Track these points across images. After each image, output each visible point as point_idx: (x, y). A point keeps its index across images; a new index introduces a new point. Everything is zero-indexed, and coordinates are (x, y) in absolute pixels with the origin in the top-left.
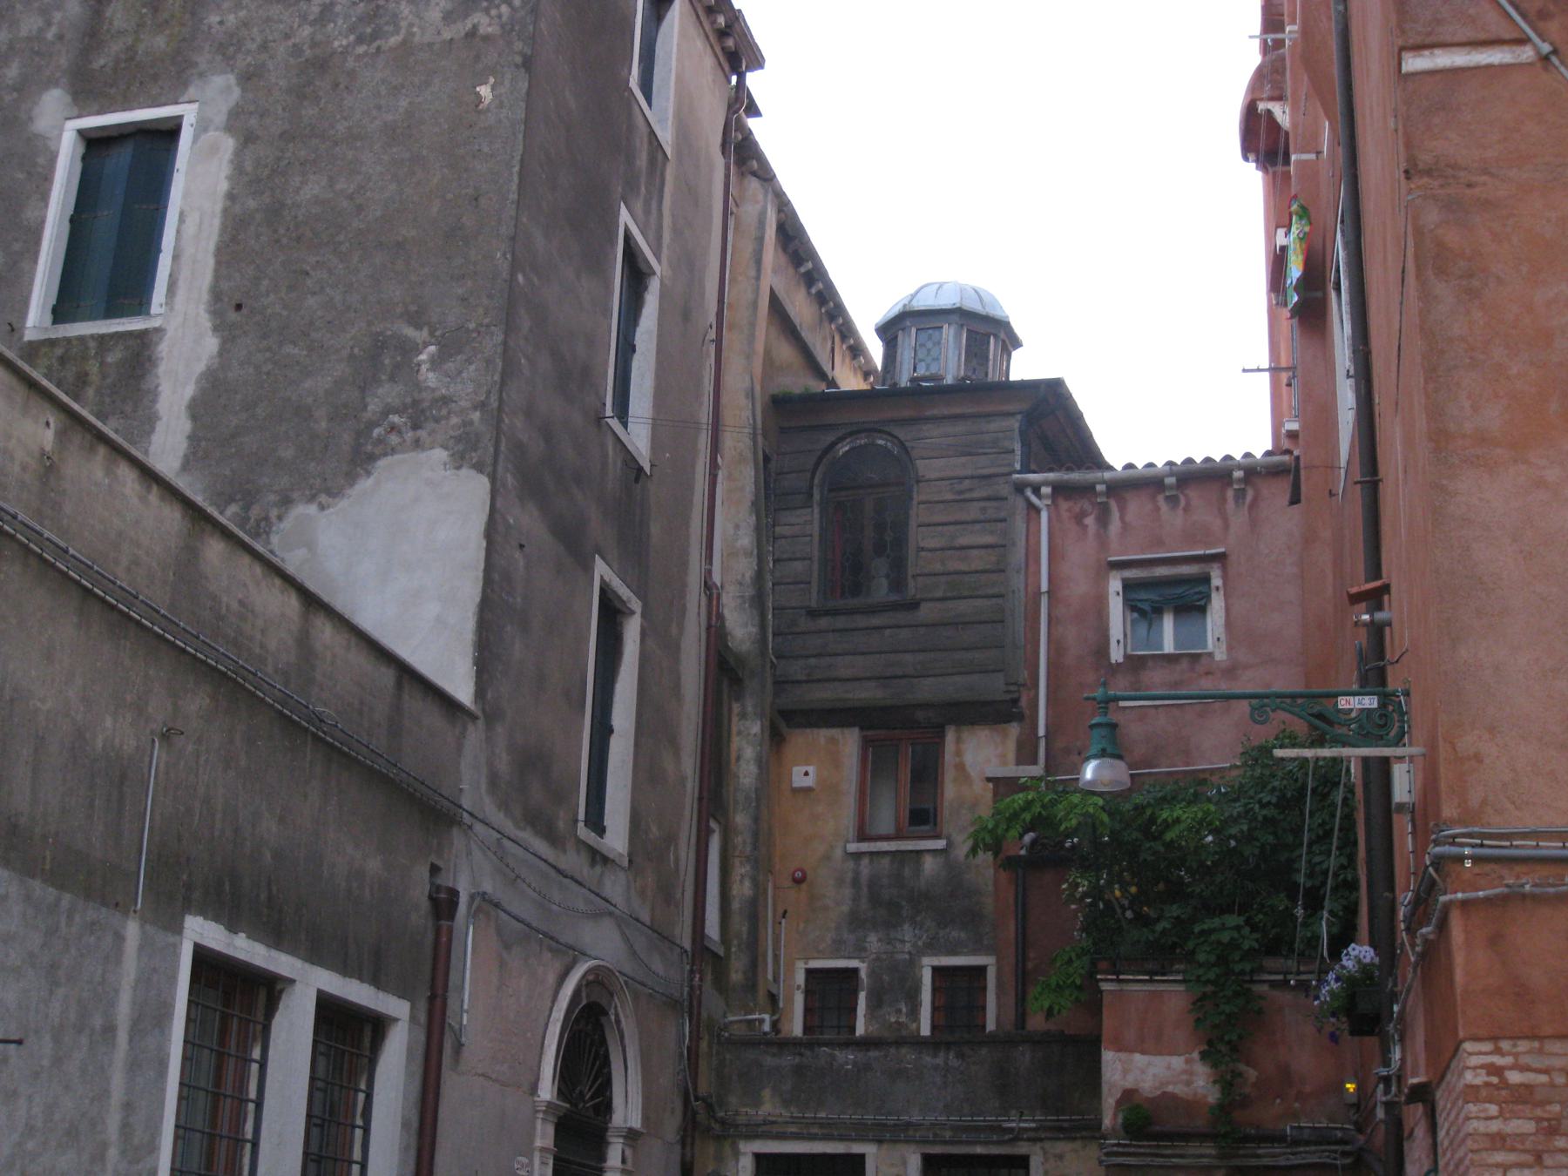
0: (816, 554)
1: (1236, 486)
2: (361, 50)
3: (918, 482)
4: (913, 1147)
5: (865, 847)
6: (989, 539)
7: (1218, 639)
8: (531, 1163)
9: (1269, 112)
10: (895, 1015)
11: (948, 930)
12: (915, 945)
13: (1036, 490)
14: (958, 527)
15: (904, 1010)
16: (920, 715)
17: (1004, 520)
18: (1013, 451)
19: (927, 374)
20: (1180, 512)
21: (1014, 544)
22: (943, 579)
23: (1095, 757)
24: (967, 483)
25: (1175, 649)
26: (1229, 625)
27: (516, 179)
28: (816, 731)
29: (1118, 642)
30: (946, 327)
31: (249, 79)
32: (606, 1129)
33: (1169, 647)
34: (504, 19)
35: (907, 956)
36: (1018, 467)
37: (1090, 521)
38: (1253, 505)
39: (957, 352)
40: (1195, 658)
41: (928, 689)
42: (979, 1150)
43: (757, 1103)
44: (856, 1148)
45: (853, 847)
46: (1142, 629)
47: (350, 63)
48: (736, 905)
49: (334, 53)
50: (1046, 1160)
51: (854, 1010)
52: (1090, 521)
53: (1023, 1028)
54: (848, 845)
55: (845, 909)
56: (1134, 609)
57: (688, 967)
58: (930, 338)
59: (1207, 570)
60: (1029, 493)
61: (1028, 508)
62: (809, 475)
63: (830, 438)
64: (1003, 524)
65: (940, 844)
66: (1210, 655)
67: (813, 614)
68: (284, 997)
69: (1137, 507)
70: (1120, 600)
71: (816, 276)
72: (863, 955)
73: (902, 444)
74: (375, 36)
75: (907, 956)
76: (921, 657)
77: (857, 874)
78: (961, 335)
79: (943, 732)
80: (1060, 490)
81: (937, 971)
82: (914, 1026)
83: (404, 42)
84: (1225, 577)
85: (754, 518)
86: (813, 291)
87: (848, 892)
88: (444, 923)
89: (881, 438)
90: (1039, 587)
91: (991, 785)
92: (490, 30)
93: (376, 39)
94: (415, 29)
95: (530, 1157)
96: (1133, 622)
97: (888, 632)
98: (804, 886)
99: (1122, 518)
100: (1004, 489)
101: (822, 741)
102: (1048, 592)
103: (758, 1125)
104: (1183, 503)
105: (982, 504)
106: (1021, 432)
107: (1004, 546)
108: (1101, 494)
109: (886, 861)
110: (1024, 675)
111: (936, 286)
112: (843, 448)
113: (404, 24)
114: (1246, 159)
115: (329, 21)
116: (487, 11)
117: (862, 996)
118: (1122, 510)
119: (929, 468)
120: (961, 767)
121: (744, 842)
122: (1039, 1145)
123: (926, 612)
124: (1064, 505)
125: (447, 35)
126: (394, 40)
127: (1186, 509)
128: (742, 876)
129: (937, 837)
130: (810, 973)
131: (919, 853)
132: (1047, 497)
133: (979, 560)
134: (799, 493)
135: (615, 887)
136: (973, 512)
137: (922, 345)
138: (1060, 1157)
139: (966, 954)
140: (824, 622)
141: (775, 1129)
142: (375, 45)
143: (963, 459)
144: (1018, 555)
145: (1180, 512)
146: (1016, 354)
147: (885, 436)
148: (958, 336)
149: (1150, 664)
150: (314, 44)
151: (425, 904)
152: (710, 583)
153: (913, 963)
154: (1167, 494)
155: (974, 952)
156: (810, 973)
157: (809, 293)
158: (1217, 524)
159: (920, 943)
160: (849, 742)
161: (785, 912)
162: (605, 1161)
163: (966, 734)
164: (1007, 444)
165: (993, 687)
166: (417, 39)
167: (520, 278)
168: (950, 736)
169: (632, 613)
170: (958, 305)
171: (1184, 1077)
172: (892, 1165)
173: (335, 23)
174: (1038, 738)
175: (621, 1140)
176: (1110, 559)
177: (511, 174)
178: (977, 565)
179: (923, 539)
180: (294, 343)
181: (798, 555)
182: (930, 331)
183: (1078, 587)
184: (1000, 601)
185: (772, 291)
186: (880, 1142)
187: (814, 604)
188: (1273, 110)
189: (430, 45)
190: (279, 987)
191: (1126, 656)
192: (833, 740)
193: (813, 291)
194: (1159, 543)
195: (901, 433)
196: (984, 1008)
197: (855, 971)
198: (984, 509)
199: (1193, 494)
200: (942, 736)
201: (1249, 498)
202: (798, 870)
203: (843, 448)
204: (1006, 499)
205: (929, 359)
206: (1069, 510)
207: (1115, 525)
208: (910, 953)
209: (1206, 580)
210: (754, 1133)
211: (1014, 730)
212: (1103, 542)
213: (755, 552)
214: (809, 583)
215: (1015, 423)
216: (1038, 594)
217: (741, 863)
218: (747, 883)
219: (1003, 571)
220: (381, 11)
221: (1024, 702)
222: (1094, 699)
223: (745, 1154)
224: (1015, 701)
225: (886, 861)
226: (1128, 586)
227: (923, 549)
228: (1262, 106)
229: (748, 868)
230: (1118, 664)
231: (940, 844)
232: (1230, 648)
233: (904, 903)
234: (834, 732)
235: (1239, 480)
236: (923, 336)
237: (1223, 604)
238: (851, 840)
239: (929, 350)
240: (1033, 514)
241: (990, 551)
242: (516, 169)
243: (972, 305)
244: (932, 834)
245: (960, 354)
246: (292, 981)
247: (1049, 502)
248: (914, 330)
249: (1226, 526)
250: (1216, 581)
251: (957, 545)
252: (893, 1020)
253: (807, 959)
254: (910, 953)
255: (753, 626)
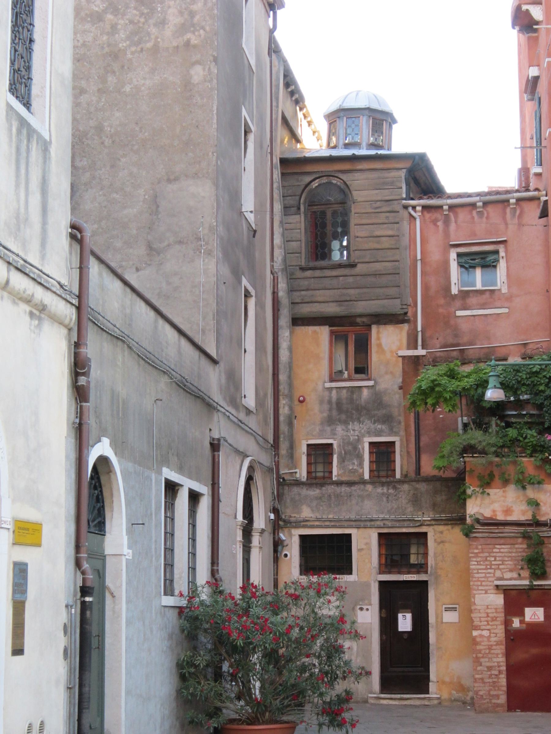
0: (303, 239)
1: (511, 207)
2: (133, 49)
3: (354, 203)
4: (374, 530)
5: (334, 385)
6: (390, 233)
7: (503, 282)
8: (236, 548)
9: (527, 10)
10: (353, 465)
11: (376, 425)
12: (360, 432)
13: (414, 208)
14: (375, 226)
15: (356, 463)
16: (359, 320)
17: (398, 223)
18: (401, 188)
19: (353, 141)
20: (484, 219)
21: (403, 235)
22: (368, 252)
23: (492, 388)
24: (378, 204)
25: (482, 286)
26: (508, 275)
27: (215, 117)
28: (307, 327)
29: (455, 284)
30: (361, 117)
31: (79, 61)
32: (252, 530)
33: (479, 286)
34: (202, 37)
35: (356, 437)
36: (404, 196)
37: (440, 224)
38: (520, 216)
39: (367, 131)
40: (492, 291)
41: (361, 307)
42: (404, 530)
43: (299, 513)
44: (347, 531)
45: (328, 385)
46: (465, 276)
47: (129, 56)
48: (281, 418)
49: (120, 50)
50: (435, 534)
51: (331, 463)
52: (440, 224)
53: (419, 474)
54: (325, 384)
55: (325, 415)
56: (462, 266)
57: (274, 453)
58: (353, 122)
59: (497, 248)
60: (410, 209)
61: (410, 219)
62: (297, 198)
63: (308, 179)
64: (398, 225)
65: (371, 383)
66: (500, 290)
67: (302, 269)
68: (179, 492)
69: (463, 215)
70: (456, 262)
71: (295, 91)
72: (335, 437)
73: (345, 183)
74: (139, 42)
75: (356, 437)
76: (358, 291)
77: (330, 397)
78: (369, 121)
79: (371, 328)
80: (425, 208)
81: (371, 444)
82: (462, 511)
83: (154, 45)
84: (506, 252)
85: (282, 229)
86: (294, 99)
87: (326, 407)
88: (216, 453)
89: (334, 180)
90: (416, 257)
91: (401, 359)
92: (196, 42)
93: (140, 43)
94: (159, 40)
95: (236, 545)
96: (461, 272)
97: (341, 278)
98: (304, 404)
99: (456, 222)
100: (398, 207)
101: (310, 332)
102: (421, 260)
103: (300, 522)
104: (486, 215)
105: (388, 214)
106: (405, 179)
107: (398, 236)
108: (446, 210)
109: (345, 391)
110: (410, 301)
111: (355, 94)
112: (315, 184)
113: (153, 37)
114: (513, 28)
115: (116, 33)
116: (193, 33)
117: (335, 457)
118: (456, 217)
119: (357, 195)
120: (379, 345)
121: (284, 388)
122: (432, 527)
123: (360, 269)
124: (427, 215)
125: (175, 44)
126: (149, 45)
127: (487, 218)
128: (284, 404)
129: (369, 379)
130: (308, 445)
131: (360, 387)
132: (419, 211)
133: (386, 243)
134: (293, 207)
135: (252, 422)
136: (382, 218)
137: (349, 126)
138: (441, 532)
139: (386, 436)
140: (309, 273)
141: (309, 524)
142: (140, 46)
143: (377, 191)
144: (405, 241)
145: (484, 219)
146: (394, 126)
147: (336, 179)
148: (368, 121)
149: (471, 295)
150: (109, 45)
151: (208, 445)
152: (273, 272)
153: (359, 440)
154: (478, 210)
155: (389, 435)
156: (308, 445)
157: (291, 100)
158: (502, 227)
159: (363, 431)
160: (324, 332)
161: (296, 417)
162: (251, 543)
163: (382, 327)
164: (399, 184)
165: (394, 306)
166: (161, 44)
167: (219, 162)
168: (374, 328)
169: (252, 296)
170: (367, 106)
171: (503, 498)
172: (365, 538)
173: (119, 34)
174: (417, 332)
175: (258, 534)
176: (451, 243)
177: (213, 114)
178: (386, 245)
179: (357, 231)
180: (117, 193)
181: (294, 239)
182: (353, 119)
183: (435, 256)
184: (397, 263)
185: (283, 114)
186: (358, 528)
187: (303, 264)
188: (530, 9)
189: (167, 49)
190: (177, 488)
191: (460, 291)
192: (315, 332)
193: (294, 99)
194: (474, 234)
195: (344, 177)
196: (394, 461)
197: (331, 445)
198: (387, 217)
199: (490, 209)
200: (370, 330)
201: (518, 212)
202: (302, 396)
203: (315, 184)
204: (398, 212)
205: (353, 134)
206: (430, 218)
207: (453, 226)
208: (357, 436)
209: (497, 252)
210: (298, 524)
211: (406, 326)
212: (446, 234)
213: (283, 247)
214: (301, 253)
215: (403, 174)
216: (416, 260)
217: (283, 398)
218: (287, 408)
219: (398, 249)
220: (141, 30)
221: (410, 314)
222: (490, 365)
223: (295, 535)
224: (406, 313)
225: (345, 391)
226: (459, 255)
227: (358, 237)
228: (524, 7)
229: (287, 400)
230: (455, 295)
231: (371, 383)
232: (509, 287)
233: (354, 412)
234: (316, 328)
235: (513, 204)
236: (350, 121)
237: (505, 265)
238: (326, 381)
239: (353, 129)
240: (412, 219)
241: (391, 238)
242: (215, 112)
243: (375, 106)
244: (367, 378)
245: (369, 132)
246: (182, 486)
247: (420, 214)
248: (345, 118)
249: (507, 228)
250: (502, 254)
251: (375, 235)
252: (351, 468)
253: (307, 440)
254: (357, 436)
255: (283, 283)
